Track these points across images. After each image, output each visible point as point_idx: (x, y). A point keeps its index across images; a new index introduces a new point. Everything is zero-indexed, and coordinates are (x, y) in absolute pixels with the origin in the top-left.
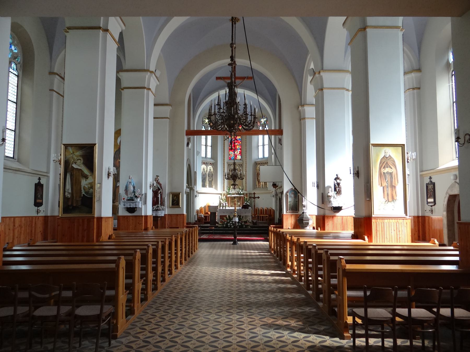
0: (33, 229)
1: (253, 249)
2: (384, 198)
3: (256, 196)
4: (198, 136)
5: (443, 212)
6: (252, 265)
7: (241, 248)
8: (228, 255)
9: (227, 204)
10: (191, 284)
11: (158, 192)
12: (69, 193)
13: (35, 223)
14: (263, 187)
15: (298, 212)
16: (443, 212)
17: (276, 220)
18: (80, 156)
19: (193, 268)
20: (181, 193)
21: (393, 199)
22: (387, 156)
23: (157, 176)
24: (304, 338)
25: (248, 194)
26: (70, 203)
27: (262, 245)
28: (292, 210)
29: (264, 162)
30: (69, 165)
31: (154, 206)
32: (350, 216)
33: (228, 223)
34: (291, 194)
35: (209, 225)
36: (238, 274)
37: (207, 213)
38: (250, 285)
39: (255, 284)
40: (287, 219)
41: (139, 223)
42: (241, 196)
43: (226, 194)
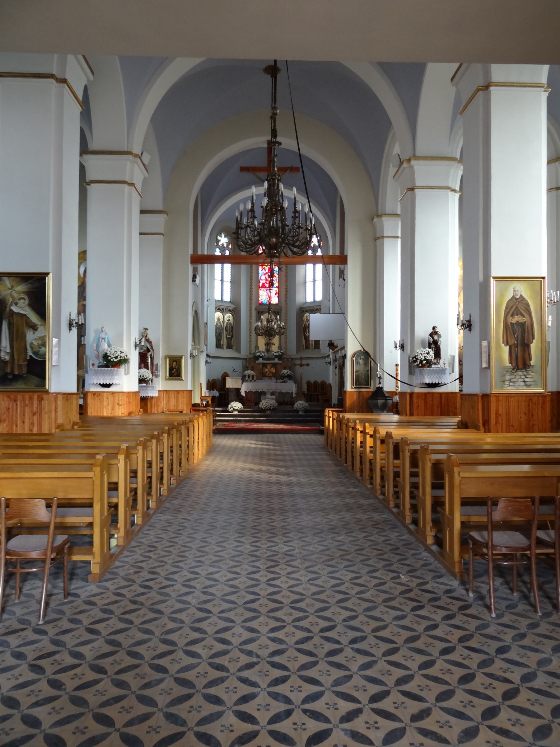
4: (209, 265)
11: (146, 355)
12: (7, 353)
15: (368, 388)
18: (24, 292)
20: (183, 358)
22: (518, 297)
23: (146, 329)
26: (9, 370)
29: (316, 308)
30: (6, 307)
41: (118, 404)
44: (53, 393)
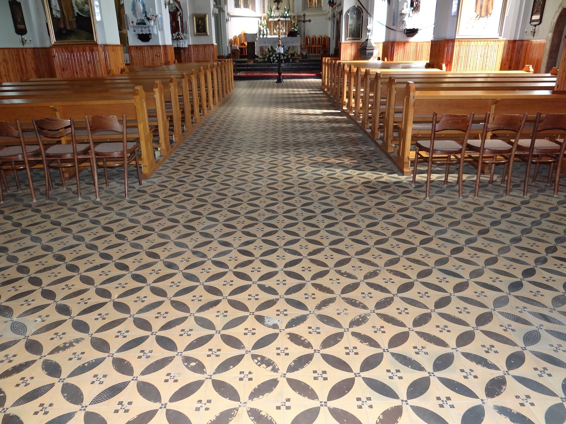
0: (23, 64)
1: (302, 88)
2: (476, 11)
3: (307, 19)
5: (549, 33)
6: (300, 104)
7: (287, 86)
8: (272, 95)
9: (268, 32)
10: (228, 125)
12: (58, 11)
13: (24, 57)
14: (315, 7)
16: (549, 33)
17: (332, 51)
19: (229, 109)
21: (487, 13)
24: (358, 175)
25: (296, 17)
26: (62, 26)
27: (313, 83)
28: (351, 37)
31: (174, 34)
32: (427, 42)
33: (270, 56)
34: (353, 13)
35: (246, 59)
36: (284, 114)
37: (243, 44)
38: (297, 125)
39: (304, 124)
40: (346, 49)
42: (287, 19)
43: (267, 18)
44: (101, 45)
